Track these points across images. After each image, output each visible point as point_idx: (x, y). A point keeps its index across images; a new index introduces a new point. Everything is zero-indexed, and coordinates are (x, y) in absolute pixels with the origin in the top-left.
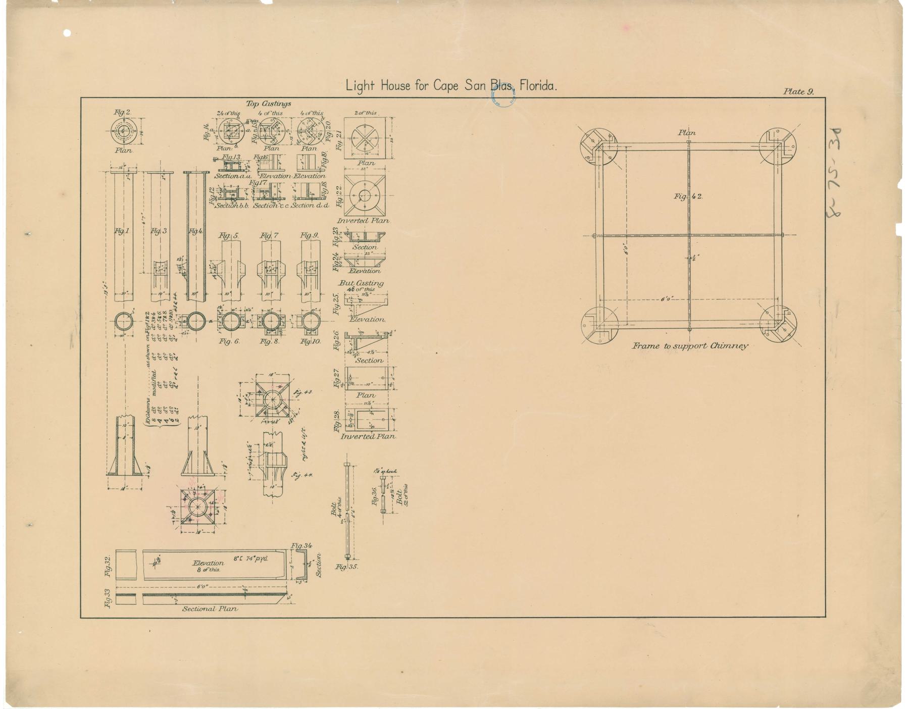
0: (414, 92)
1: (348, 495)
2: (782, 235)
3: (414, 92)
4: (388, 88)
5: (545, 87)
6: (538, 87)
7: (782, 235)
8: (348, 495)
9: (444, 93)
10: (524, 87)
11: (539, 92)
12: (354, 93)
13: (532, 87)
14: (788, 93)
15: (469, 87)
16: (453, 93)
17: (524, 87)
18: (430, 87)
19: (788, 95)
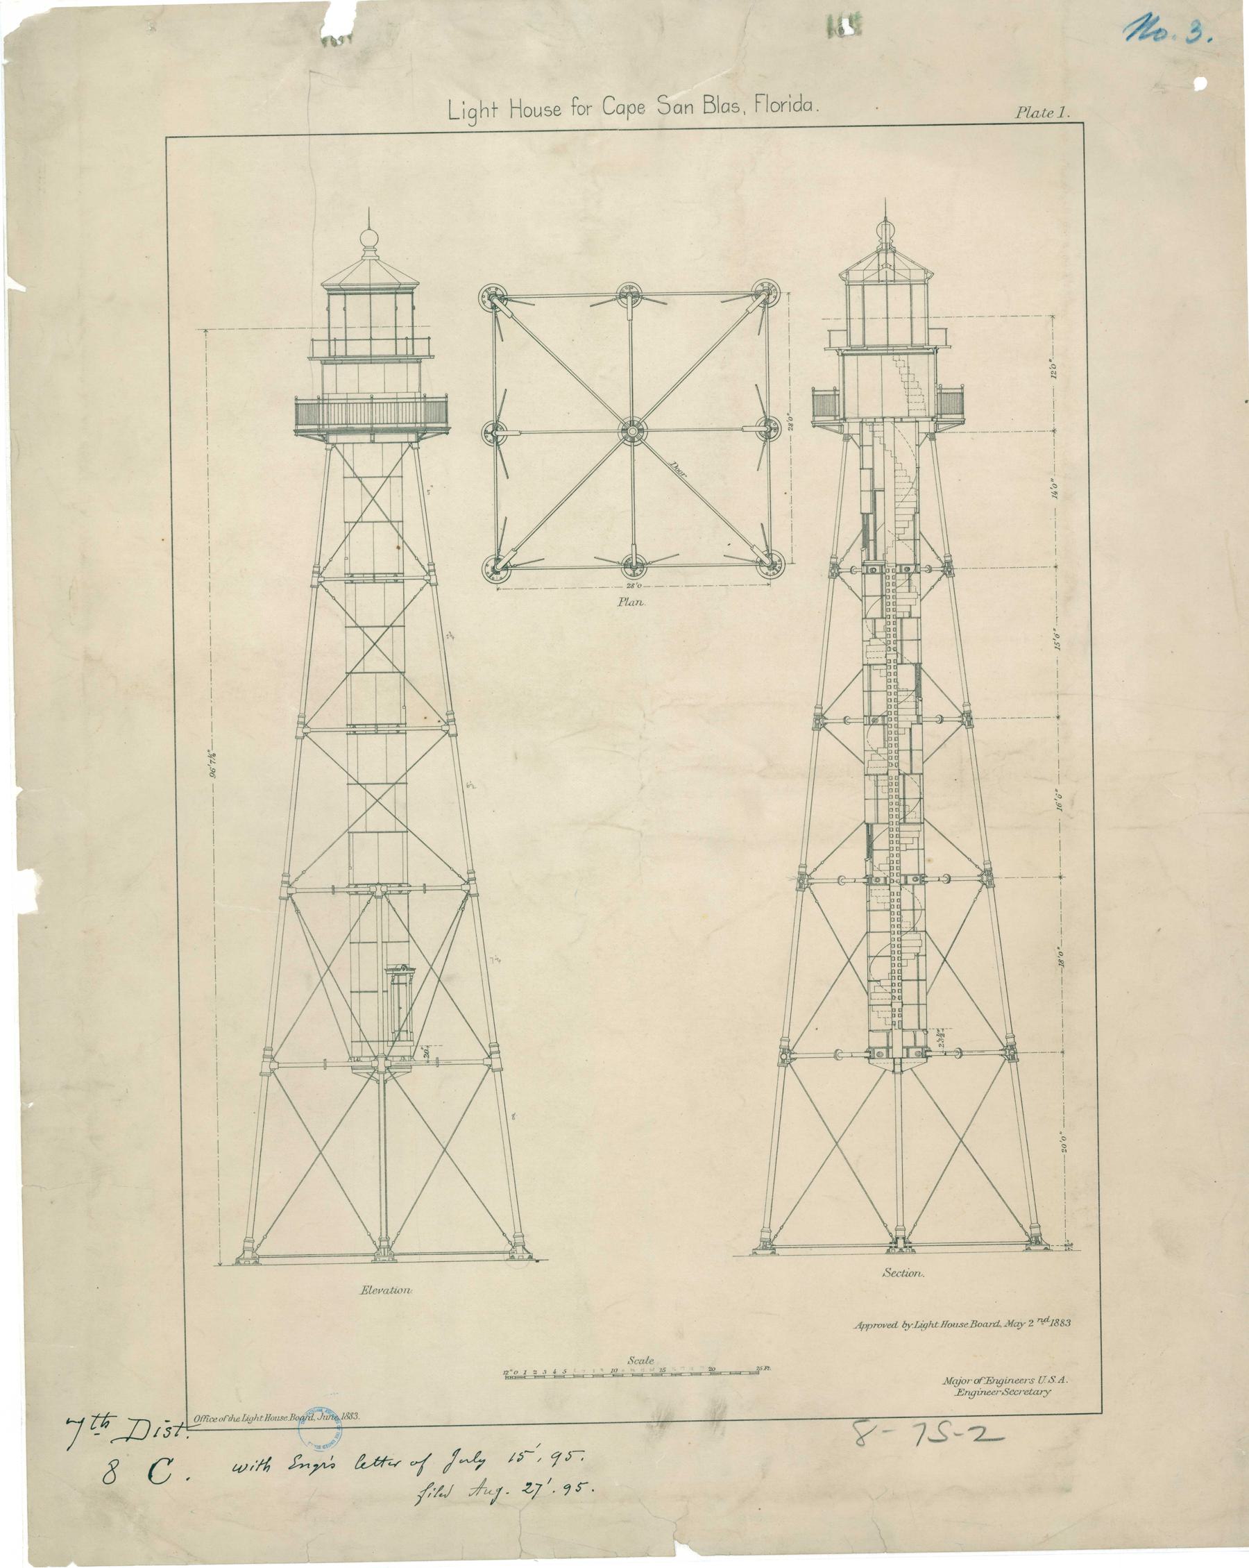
0: (568, 119)
1: (718, 293)
2: (869, 880)
3: (568, 119)
4: (770, 108)
5: (798, 106)
6: (786, 106)
7: (869, 880)
8: (718, 293)
9: (618, 121)
10: (762, 107)
11: (786, 117)
12: (462, 125)
13: (775, 107)
14: (1023, 115)
15: (665, 108)
16: (636, 120)
17: (762, 107)
18: (567, 111)
19: (1023, 118)
